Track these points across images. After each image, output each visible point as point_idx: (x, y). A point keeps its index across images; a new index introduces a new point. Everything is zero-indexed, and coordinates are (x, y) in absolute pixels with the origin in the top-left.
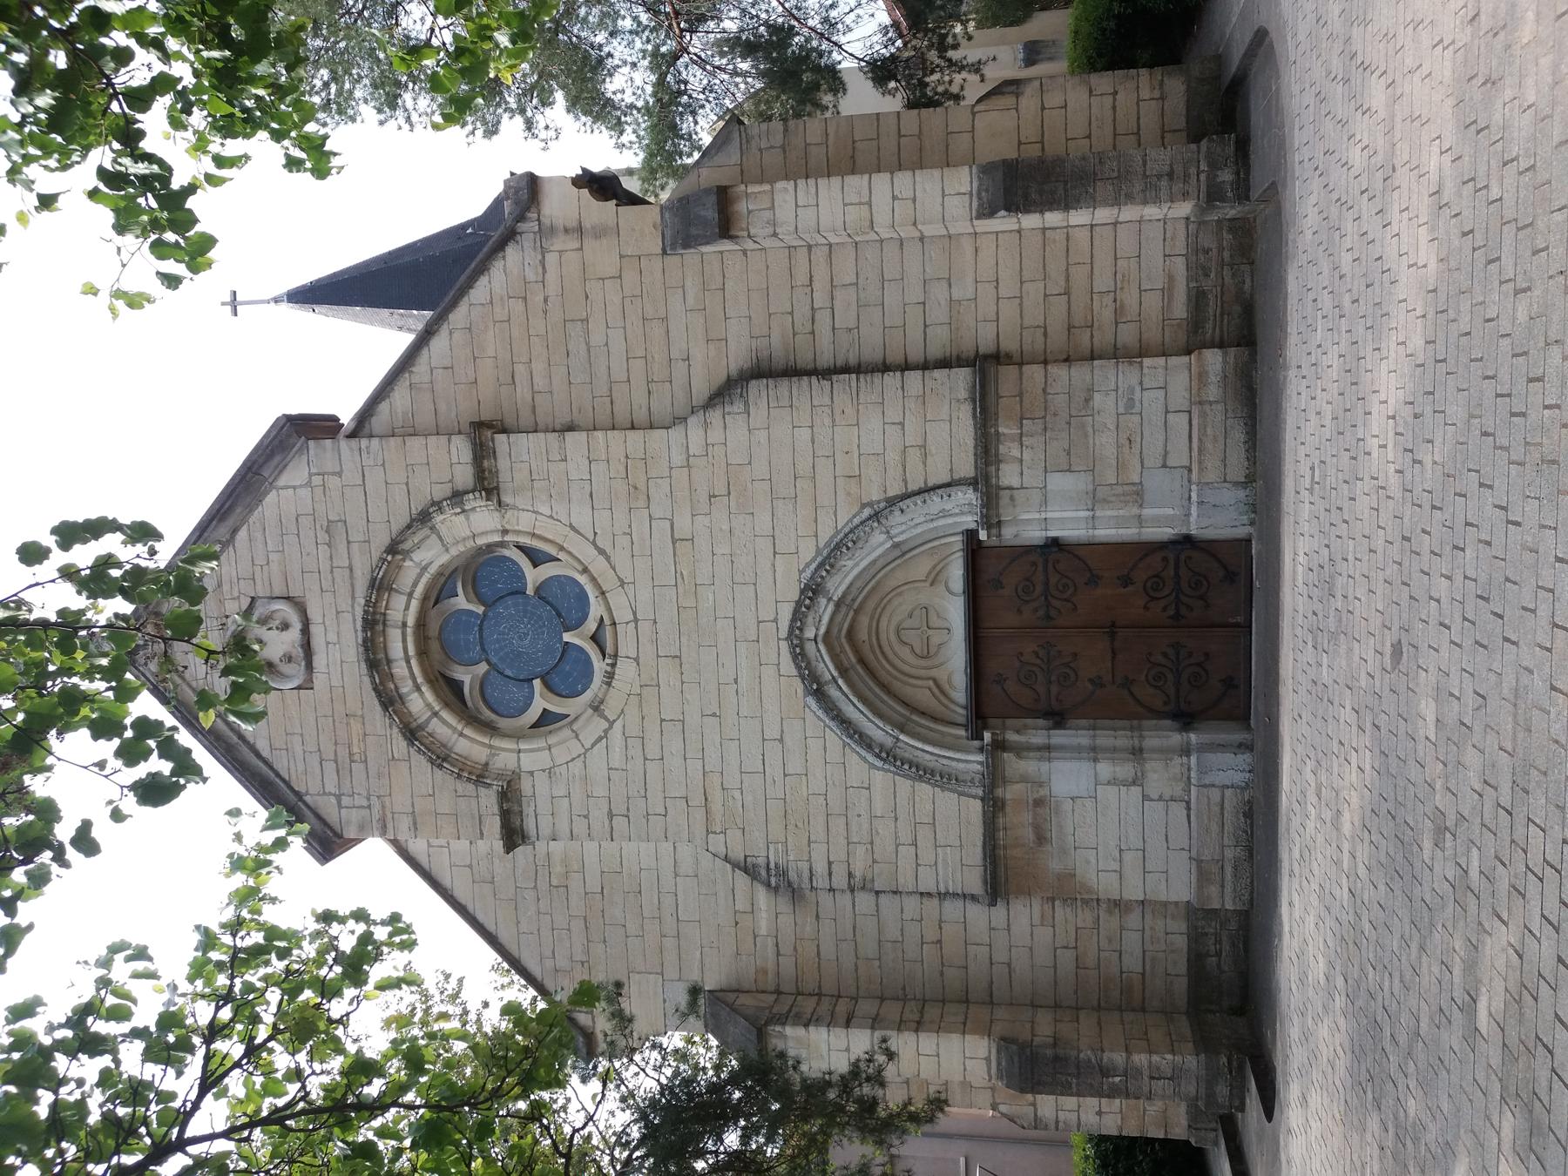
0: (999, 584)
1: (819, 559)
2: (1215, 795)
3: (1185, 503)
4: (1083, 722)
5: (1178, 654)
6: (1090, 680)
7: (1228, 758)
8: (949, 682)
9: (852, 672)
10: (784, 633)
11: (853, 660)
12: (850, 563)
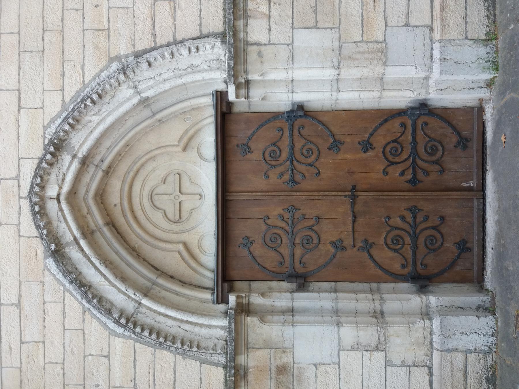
0: (247, 149)
1: (65, 114)
2: (458, 359)
3: (428, 62)
4: (325, 285)
5: (415, 217)
6: (333, 243)
7: (470, 321)
8: (200, 246)
9: (98, 235)
10: (25, 192)
11: (100, 221)
12: (96, 119)
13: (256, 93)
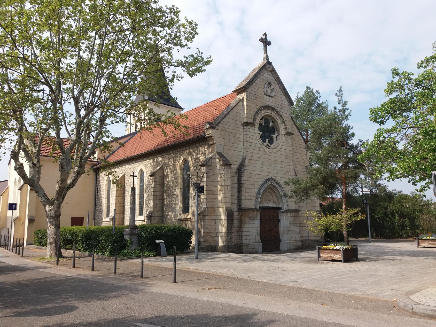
2: (257, 247)
13: (282, 214)
